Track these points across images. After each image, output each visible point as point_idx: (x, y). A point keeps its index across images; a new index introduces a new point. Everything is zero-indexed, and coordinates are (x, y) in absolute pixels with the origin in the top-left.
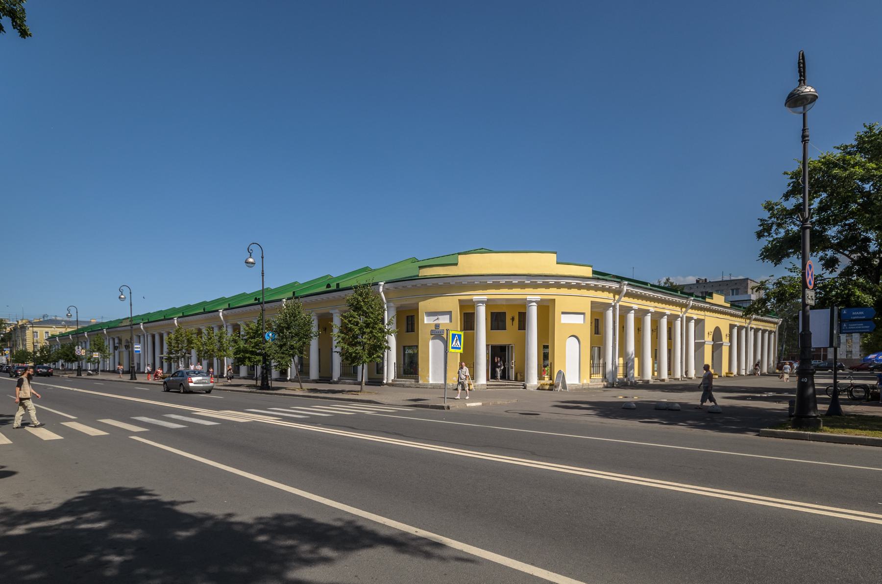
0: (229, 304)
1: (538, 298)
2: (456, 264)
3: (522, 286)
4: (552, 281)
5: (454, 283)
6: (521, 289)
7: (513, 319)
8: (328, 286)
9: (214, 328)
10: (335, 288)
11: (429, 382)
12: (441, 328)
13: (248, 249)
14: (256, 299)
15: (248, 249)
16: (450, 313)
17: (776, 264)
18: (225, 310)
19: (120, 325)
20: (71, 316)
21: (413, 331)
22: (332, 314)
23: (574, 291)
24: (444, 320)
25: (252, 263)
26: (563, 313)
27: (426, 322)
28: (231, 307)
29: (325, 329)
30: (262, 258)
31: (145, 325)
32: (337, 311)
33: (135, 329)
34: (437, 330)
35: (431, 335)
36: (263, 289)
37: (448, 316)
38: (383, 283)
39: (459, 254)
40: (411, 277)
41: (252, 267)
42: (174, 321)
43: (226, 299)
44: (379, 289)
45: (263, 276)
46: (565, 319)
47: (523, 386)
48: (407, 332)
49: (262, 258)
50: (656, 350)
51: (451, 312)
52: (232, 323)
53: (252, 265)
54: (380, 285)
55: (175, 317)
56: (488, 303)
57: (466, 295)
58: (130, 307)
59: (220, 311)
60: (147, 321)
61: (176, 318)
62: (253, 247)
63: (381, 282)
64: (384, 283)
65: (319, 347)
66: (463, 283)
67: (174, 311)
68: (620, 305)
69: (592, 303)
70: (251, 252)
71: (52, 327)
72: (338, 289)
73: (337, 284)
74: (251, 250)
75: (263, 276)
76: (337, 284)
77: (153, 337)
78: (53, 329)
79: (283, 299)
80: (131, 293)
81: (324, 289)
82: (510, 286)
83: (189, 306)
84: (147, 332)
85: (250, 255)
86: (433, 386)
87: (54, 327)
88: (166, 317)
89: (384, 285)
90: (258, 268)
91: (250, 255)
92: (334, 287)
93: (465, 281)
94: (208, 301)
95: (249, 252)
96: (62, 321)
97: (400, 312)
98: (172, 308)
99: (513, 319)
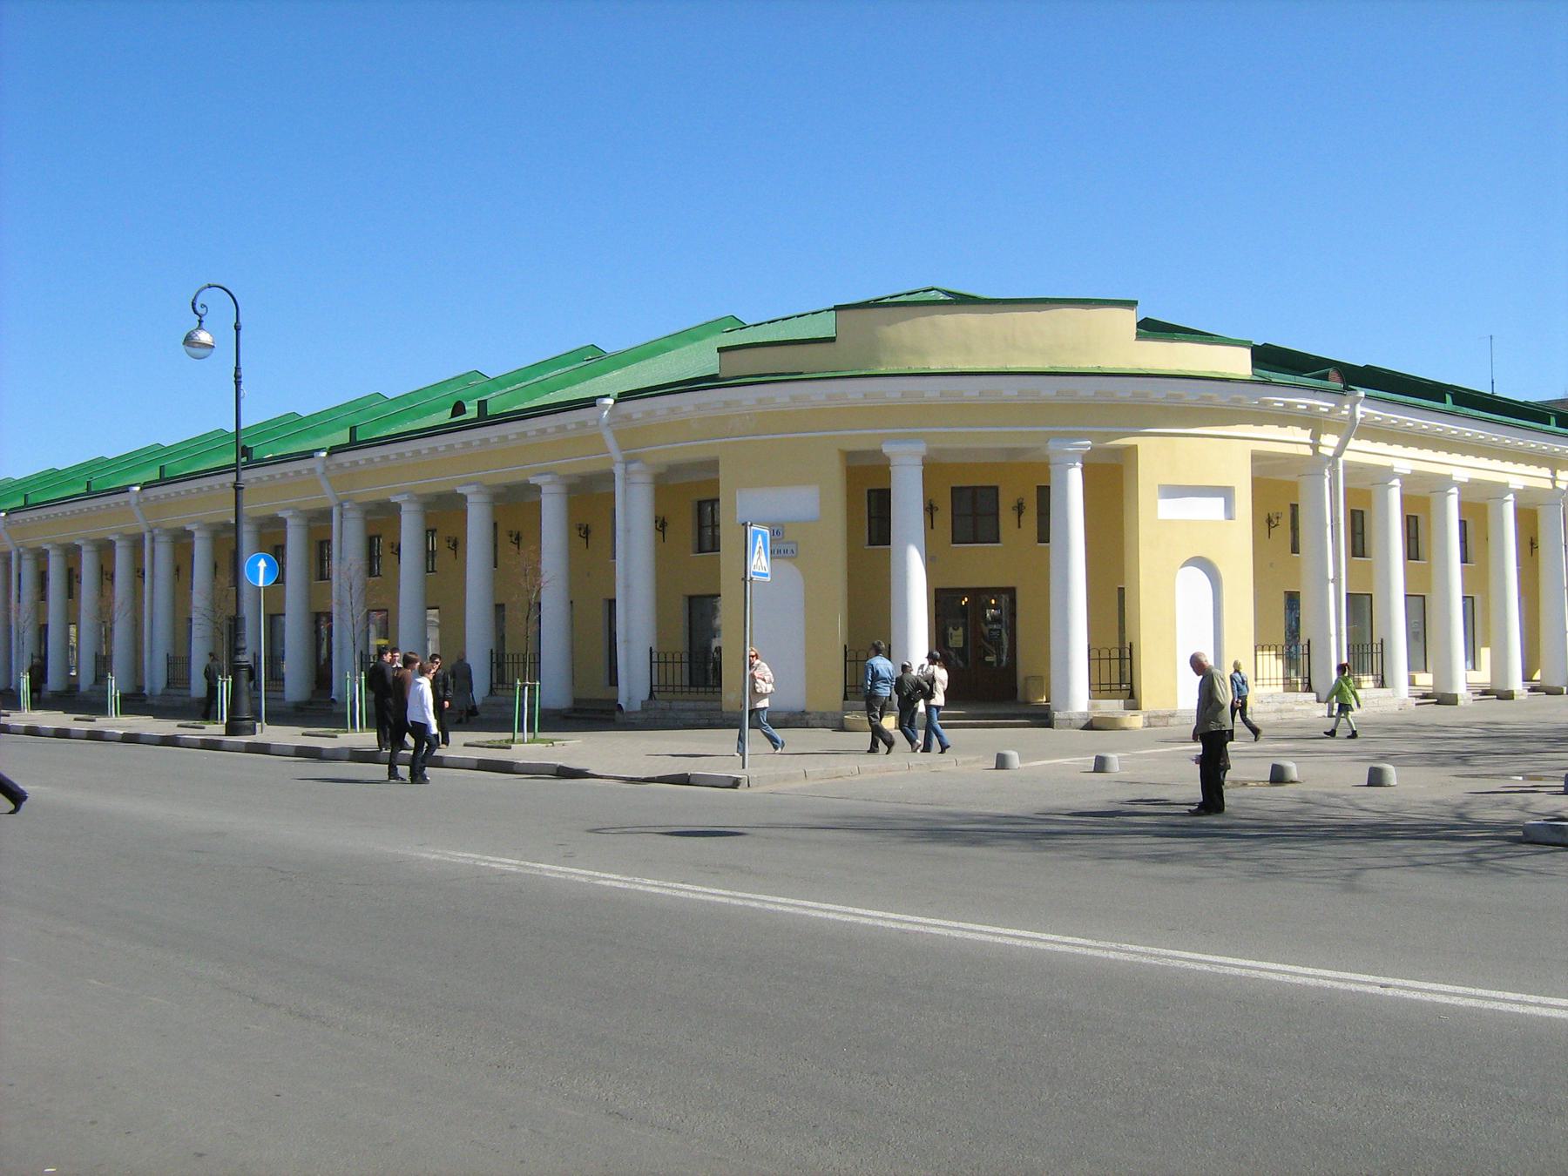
0: (162, 469)
2: (720, 350)
7: (1020, 508)
8: (459, 408)
13: (193, 304)
16: (1226, 493)
29: (518, 538)
30: (237, 328)
38: (610, 401)
45: (238, 383)
46: (1169, 509)
48: (700, 551)
49: (237, 328)
50: (1292, 600)
62: (208, 298)
65: (174, 560)
68: (1344, 462)
69: (1256, 457)
72: (485, 419)
74: (203, 306)
75: (238, 383)
81: (444, 417)
83: (54, 472)
85: (200, 322)
91: (200, 322)
95: (196, 312)
97: (666, 484)
99: (1020, 508)
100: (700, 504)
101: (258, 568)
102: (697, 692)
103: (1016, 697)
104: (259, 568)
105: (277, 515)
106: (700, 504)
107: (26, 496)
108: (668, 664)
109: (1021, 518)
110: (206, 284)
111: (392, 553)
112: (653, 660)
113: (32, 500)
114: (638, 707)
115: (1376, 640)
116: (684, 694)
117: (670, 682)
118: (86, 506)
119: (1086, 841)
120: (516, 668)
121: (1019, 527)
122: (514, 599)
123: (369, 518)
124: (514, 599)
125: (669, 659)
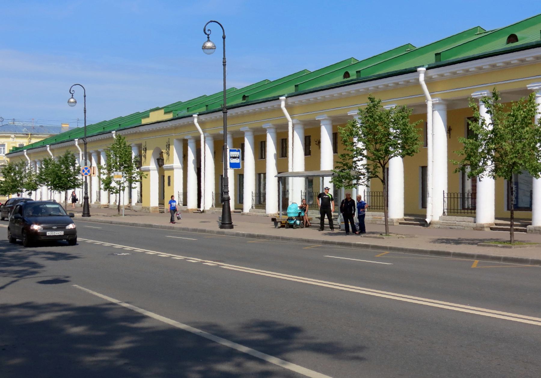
8: (347, 75)
9: (189, 141)
13: (204, 30)
14: (244, 97)
15: (204, 30)
19: (144, 121)
20: (76, 102)
25: (211, 48)
33: (233, 117)
36: (85, 127)
41: (73, 106)
42: (47, 149)
43: (123, 118)
44: (280, 105)
45: (224, 65)
52: (303, 118)
53: (211, 51)
55: (194, 114)
58: (84, 113)
67: (112, 123)
70: (208, 33)
71: (9, 137)
74: (209, 30)
75: (85, 113)
78: (11, 139)
80: (224, 38)
81: (340, 79)
85: (208, 38)
87: (13, 136)
91: (208, 38)
92: (353, 76)
95: (206, 34)
96: (24, 127)
100: (262, 142)
105: (98, 150)
106: (262, 142)
108: (379, 195)
111: (316, 144)
113: (302, 89)
116: (462, 213)
117: (456, 208)
118: (98, 138)
119: (344, 247)
125: (456, 196)
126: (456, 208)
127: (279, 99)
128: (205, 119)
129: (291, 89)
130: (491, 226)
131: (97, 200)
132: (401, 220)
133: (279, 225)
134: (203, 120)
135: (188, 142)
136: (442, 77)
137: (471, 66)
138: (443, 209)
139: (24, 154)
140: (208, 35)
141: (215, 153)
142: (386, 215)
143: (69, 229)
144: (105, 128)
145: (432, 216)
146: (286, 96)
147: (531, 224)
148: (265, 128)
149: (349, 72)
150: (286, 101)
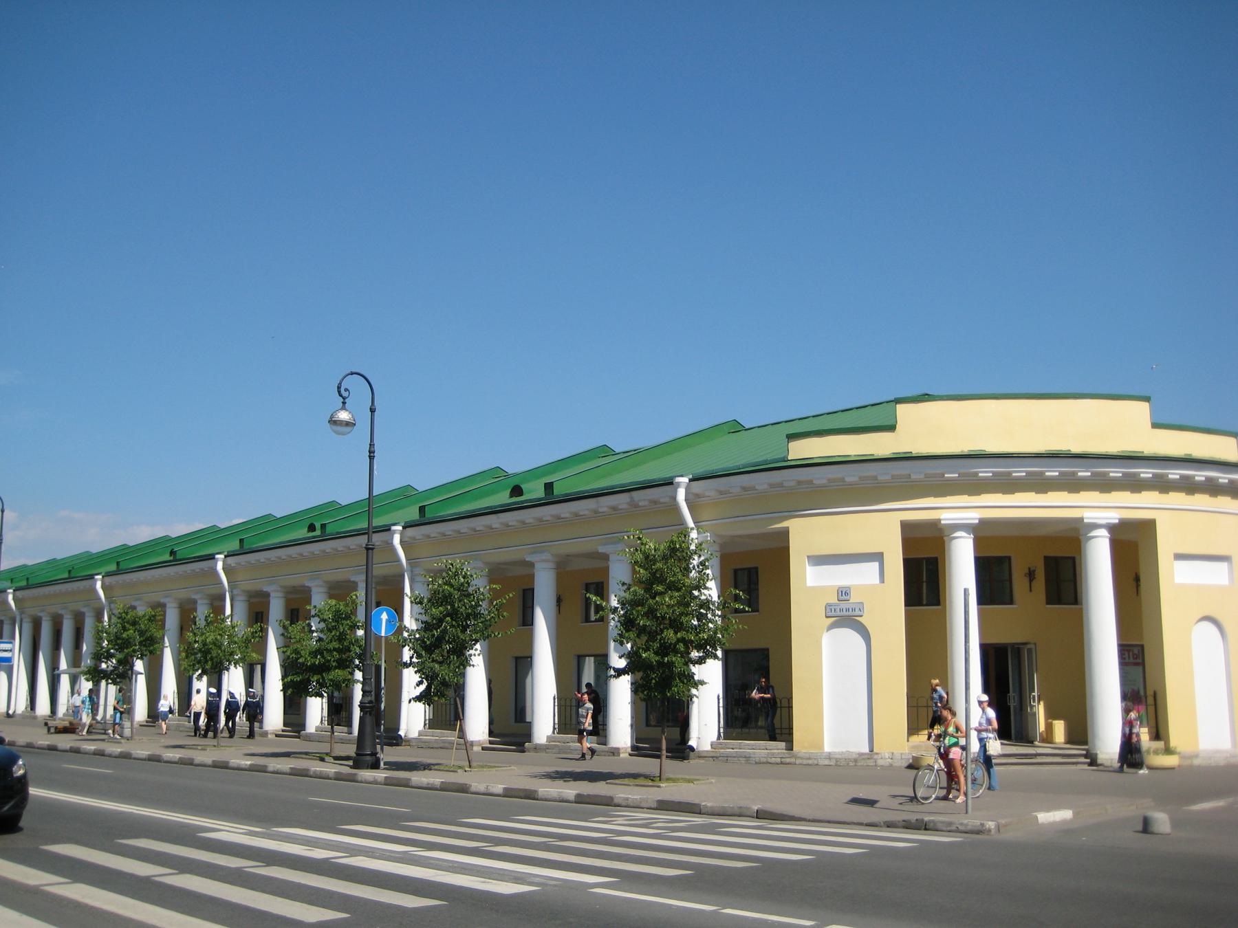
0: (241, 541)
1: (1113, 517)
2: (891, 428)
3: (1073, 485)
4: (1146, 473)
5: (922, 476)
6: (1003, 494)
10: (540, 493)
11: (822, 747)
12: (854, 598)
13: (339, 388)
15: (339, 388)
17: (1029, 569)
18: (108, 574)
21: (938, 603)
22: (531, 565)
23: (1202, 501)
24: (862, 576)
25: (347, 424)
26: (1179, 557)
27: (810, 583)
28: (247, 546)
30: (372, 411)
31: (18, 593)
32: (546, 556)
34: (844, 605)
35: (827, 617)
37: (876, 565)
38: (685, 480)
39: (899, 401)
40: (766, 462)
41: (343, 434)
45: (371, 458)
47: (1086, 756)
49: (372, 411)
51: (882, 554)
54: (679, 484)
56: (984, 533)
57: (923, 509)
59: (394, 528)
60: (24, 583)
61: (100, 577)
63: (682, 476)
64: (690, 480)
66: (847, 479)
67: (214, 535)
70: (345, 394)
72: (550, 497)
73: (546, 484)
74: (346, 390)
75: (371, 458)
76: (546, 484)
77: (37, 625)
79: (395, 524)
82: (1041, 485)
84: (22, 613)
85: (344, 403)
86: (837, 760)
88: (31, 582)
89: (688, 484)
90: (361, 435)
91: (344, 403)
92: (534, 490)
93: (917, 472)
94: (173, 536)
95: (341, 395)
98: (48, 562)
99: (1031, 575)
101: (381, 620)
102: (781, 734)
103: (528, 736)
104: (382, 619)
106: (525, 591)
107: (28, 579)
109: (1032, 585)
110: (349, 372)
112: (1153, 707)
114: (708, 747)
115: (1150, 692)
120: (448, 716)
121: (1031, 590)
122: (708, 647)
123: (251, 601)
124: (708, 647)
125: (568, 703)
126: (448, 719)
127: (389, 530)
128: (236, 563)
129: (234, 545)
130: (278, 733)
131: (26, 708)
132: (279, 731)
133: (52, 730)
134: (233, 565)
135: (312, 593)
136: (655, 504)
137: (463, 525)
138: (552, 725)
139: (95, 587)
140: (344, 398)
141: (559, 601)
142: (462, 734)
143: (17, 777)
144: (121, 563)
145: (699, 738)
146: (226, 553)
147: (304, 730)
148: (266, 592)
149: (522, 486)
150: (402, 534)
